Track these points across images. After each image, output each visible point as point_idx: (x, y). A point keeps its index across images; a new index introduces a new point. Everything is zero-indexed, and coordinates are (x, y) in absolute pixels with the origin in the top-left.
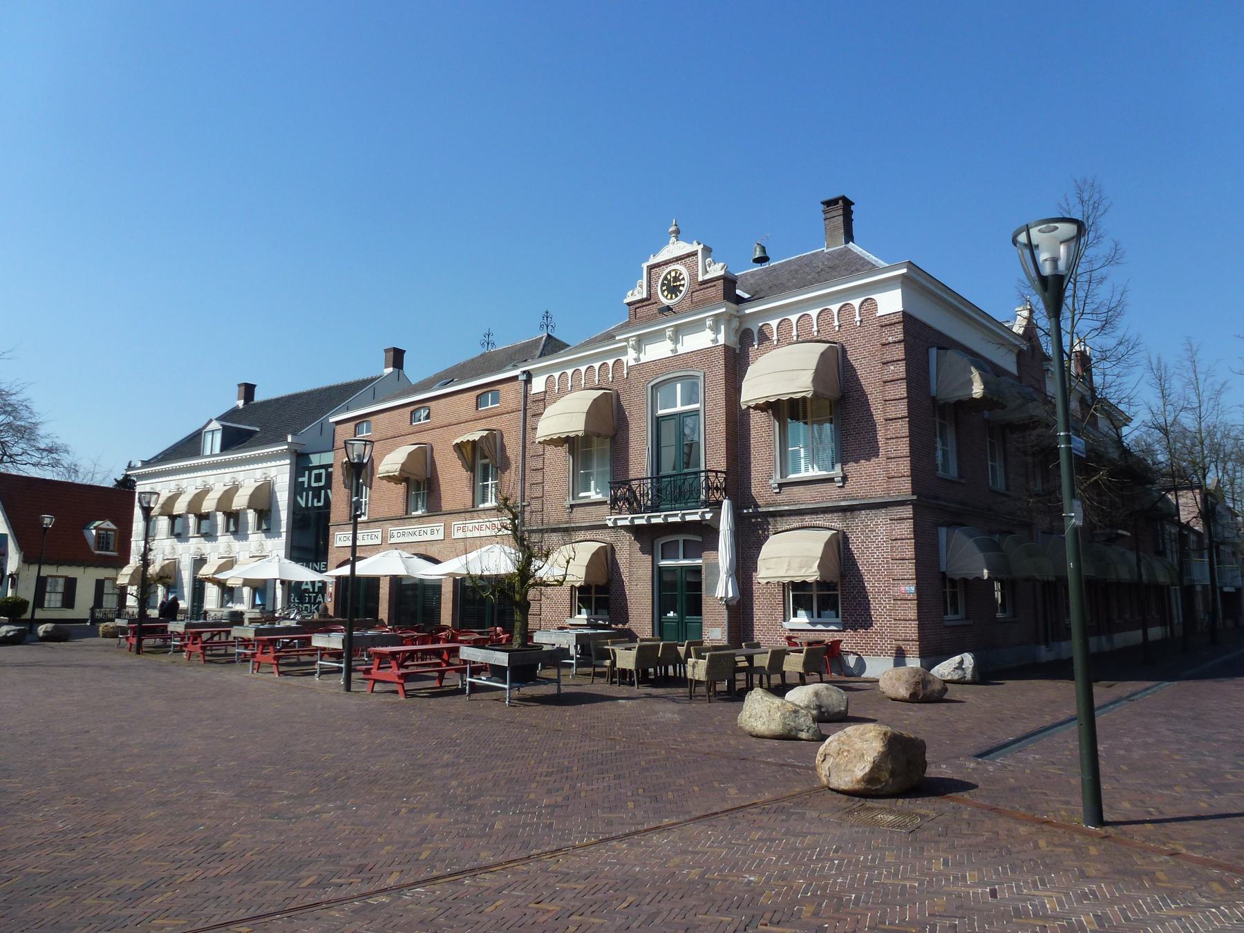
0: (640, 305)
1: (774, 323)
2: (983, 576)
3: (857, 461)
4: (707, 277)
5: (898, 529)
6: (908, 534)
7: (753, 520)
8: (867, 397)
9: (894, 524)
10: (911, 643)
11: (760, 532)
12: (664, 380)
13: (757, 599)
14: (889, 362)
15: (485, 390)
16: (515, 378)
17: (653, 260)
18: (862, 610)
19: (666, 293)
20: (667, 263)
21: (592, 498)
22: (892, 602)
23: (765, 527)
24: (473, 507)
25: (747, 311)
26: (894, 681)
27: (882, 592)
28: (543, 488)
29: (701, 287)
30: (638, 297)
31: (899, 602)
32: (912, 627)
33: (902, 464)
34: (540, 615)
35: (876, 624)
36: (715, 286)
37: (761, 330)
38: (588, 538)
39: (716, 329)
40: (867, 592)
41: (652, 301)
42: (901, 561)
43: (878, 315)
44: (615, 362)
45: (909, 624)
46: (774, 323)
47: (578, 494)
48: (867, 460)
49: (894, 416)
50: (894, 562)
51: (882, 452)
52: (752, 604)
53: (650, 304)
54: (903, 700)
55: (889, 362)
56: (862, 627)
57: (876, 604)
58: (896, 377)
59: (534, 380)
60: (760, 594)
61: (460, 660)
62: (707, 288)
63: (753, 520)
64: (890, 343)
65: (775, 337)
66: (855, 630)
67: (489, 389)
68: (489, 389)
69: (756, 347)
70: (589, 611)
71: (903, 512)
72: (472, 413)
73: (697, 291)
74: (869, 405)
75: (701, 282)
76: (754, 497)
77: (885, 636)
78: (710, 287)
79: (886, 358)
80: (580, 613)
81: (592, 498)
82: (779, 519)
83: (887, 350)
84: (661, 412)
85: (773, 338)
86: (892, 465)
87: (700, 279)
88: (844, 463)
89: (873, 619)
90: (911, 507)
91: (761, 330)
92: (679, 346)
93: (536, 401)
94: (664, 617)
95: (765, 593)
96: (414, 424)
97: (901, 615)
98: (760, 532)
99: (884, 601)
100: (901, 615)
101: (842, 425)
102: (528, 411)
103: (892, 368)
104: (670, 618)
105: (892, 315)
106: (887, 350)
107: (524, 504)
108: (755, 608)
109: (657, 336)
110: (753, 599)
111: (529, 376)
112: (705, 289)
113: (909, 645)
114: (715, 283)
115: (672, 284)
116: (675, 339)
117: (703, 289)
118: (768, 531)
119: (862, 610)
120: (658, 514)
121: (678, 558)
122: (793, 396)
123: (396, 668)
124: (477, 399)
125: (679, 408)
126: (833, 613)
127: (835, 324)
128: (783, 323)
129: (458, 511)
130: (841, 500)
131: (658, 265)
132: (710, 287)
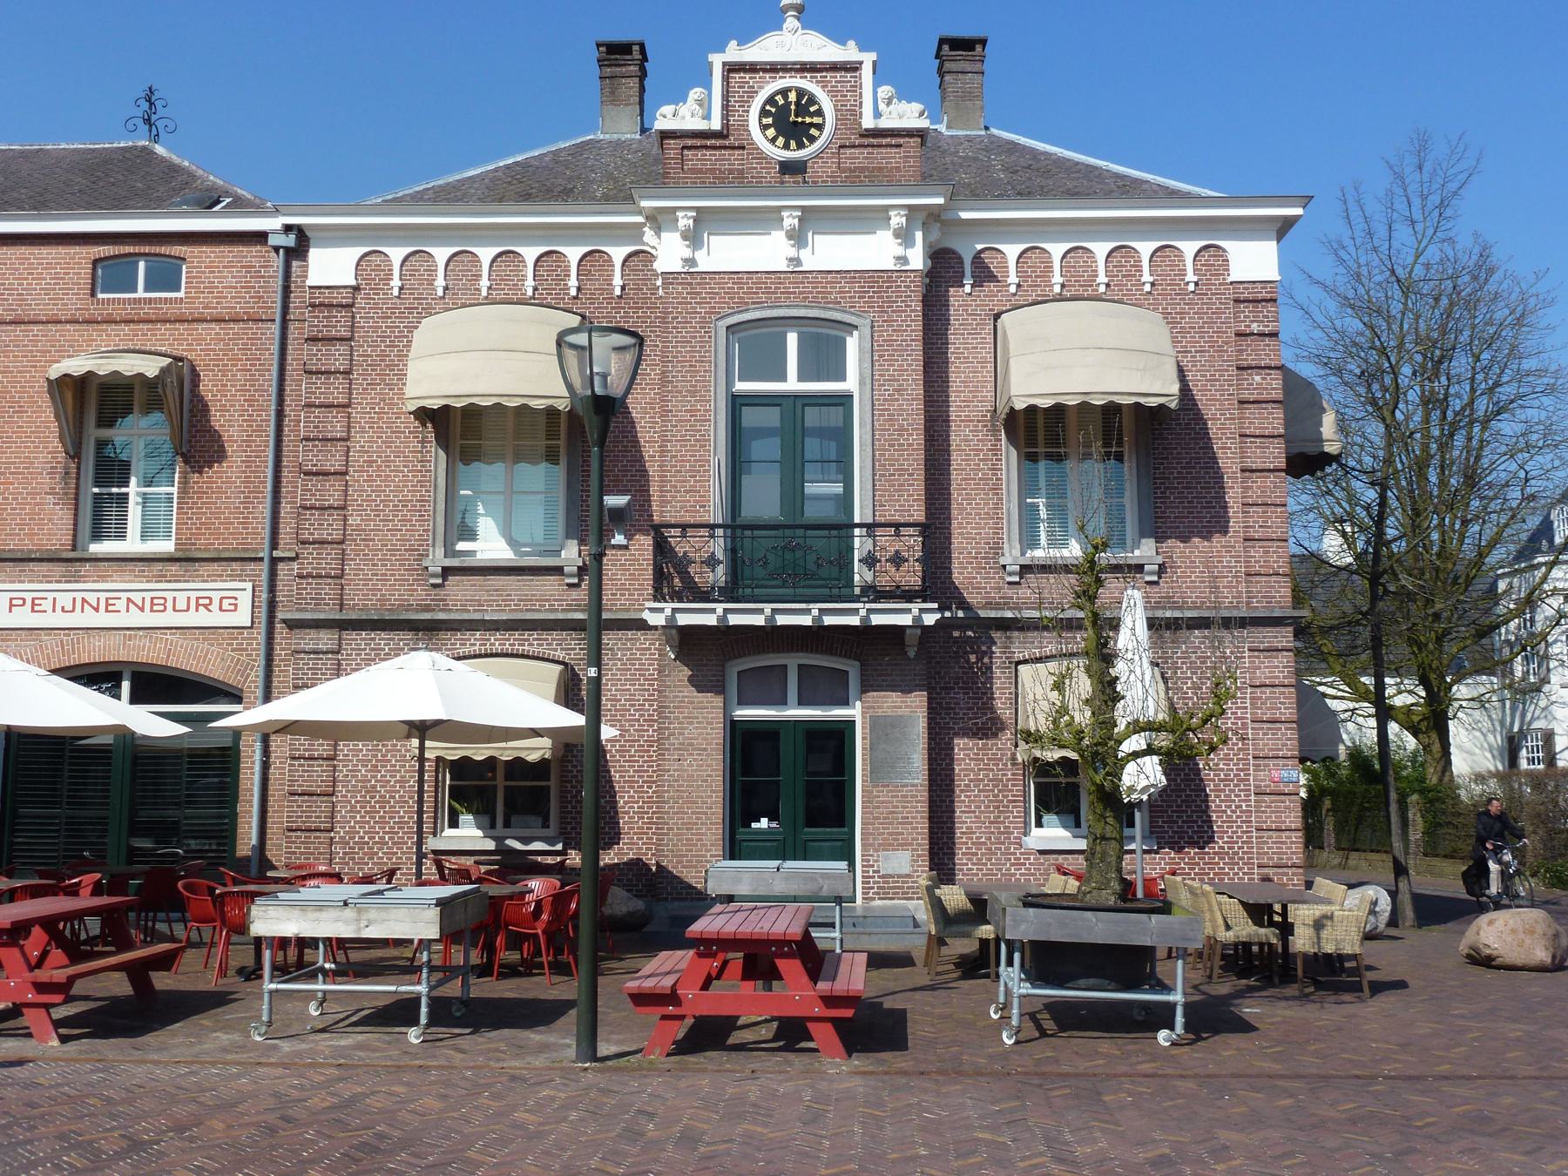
0: (698, 142)
1: (1012, 251)
2: (1338, 755)
3: (1185, 539)
4: (884, 123)
5: (1266, 667)
6: (1284, 677)
7: (956, 634)
8: (1206, 424)
9: (1259, 657)
10: (1290, 871)
11: (973, 658)
12: (738, 324)
13: (962, 791)
14: (1252, 368)
15: (137, 249)
16: (260, 237)
17: (735, 53)
18: (1192, 811)
19: (771, 132)
20: (774, 68)
21: (479, 556)
22: (1253, 797)
23: (984, 648)
24: (74, 548)
25: (964, 215)
26: (1521, 936)
27: (1232, 780)
28: (345, 520)
29: (866, 141)
30: (699, 125)
31: (1266, 798)
32: (1292, 843)
33: (1274, 552)
34: (331, 830)
35: (1222, 838)
36: (899, 146)
37: (978, 258)
38: (497, 648)
39: (904, 236)
40: (1202, 780)
41: (731, 141)
42: (1269, 725)
43: (1230, 279)
44: (585, 256)
45: (1287, 837)
46: (1012, 251)
47: (454, 544)
48: (1203, 538)
49: (1260, 466)
50: (1257, 725)
51: (1234, 524)
52: (953, 802)
53: (725, 148)
54: (1541, 969)
55: (1252, 368)
56: (1193, 844)
57: (1221, 801)
58: (1264, 396)
59: (314, 254)
60: (970, 781)
61: (258, 941)
62: (880, 146)
63: (956, 634)
64: (1253, 334)
65: (1013, 279)
66: (1180, 850)
67: (147, 249)
68: (147, 249)
69: (968, 289)
70: (486, 820)
71: (1276, 637)
72: (74, 301)
73: (854, 146)
74: (1210, 439)
75: (866, 130)
76: (957, 588)
77: (1240, 858)
78: (887, 146)
79: (1246, 360)
80: (454, 824)
81: (479, 556)
82: (1016, 634)
83: (1247, 345)
84: (741, 386)
85: (570, 284)
86: (1256, 552)
87: (868, 122)
88: (1160, 539)
89: (1215, 828)
90: (1290, 629)
91: (978, 258)
92: (700, 256)
93: (321, 305)
94: (742, 830)
95: (982, 780)
96: (100, 296)
97: (1272, 822)
98: (973, 658)
99: (1236, 796)
100: (1272, 822)
101: (1155, 469)
102: (291, 327)
103: (1258, 378)
104: (760, 831)
105: (1259, 286)
106: (1247, 345)
107: (275, 554)
108: (958, 810)
109: (762, 221)
110: (953, 791)
111: (300, 244)
112: (873, 146)
113: (1287, 874)
114: (901, 141)
115: (792, 118)
116: (798, 237)
117: (868, 146)
118: (991, 658)
119: (1192, 811)
120: (803, 606)
121: (785, 703)
122: (1142, 400)
123: (805, 979)
124: (94, 269)
125: (792, 384)
126: (539, 821)
127: (1143, 279)
128: (1029, 254)
129: (19, 555)
130: (576, 610)
131: (752, 68)
132: (887, 146)
